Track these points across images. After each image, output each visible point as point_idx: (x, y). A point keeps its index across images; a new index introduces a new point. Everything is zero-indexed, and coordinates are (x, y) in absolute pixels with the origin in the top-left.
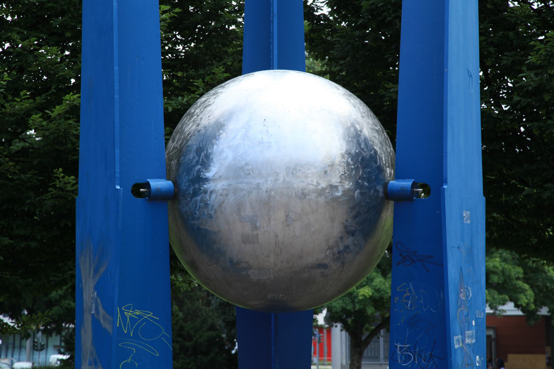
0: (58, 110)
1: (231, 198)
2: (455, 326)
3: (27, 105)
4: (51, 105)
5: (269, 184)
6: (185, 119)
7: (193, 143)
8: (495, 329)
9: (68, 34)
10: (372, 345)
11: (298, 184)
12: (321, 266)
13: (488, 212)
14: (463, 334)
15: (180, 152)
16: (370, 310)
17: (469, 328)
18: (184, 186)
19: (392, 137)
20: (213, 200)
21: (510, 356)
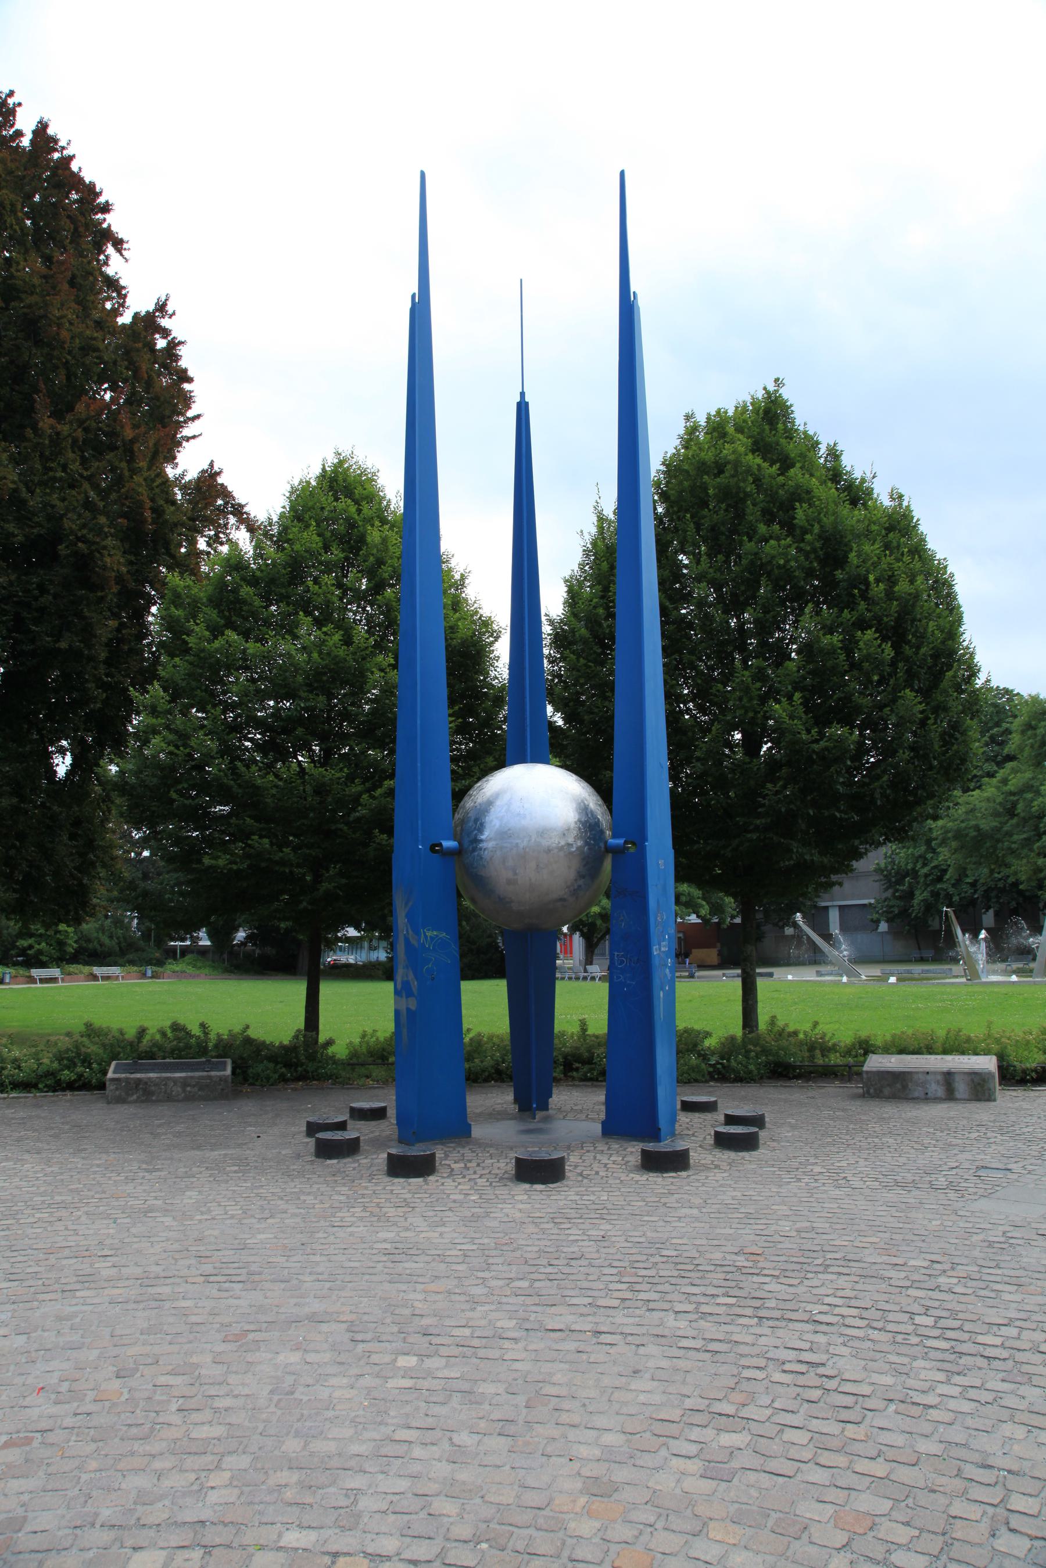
0: (379, 791)
1: (498, 853)
2: (654, 937)
3: (359, 788)
4: (375, 788)
5: (525, 843)
6: (466, 798)
7: (472, 815)
8: (684, 932)
9: (387, 740)
10: (600, 946)
11: (545, 843)
12: (562, 900)
13: (676, 858)
14: (659, 945)
15: (463, 822)
16: (599, 922)
17: (664, 940)
18: (466, 844)
19: (610, 810)
20: (486, 855)
21: (694, 950)
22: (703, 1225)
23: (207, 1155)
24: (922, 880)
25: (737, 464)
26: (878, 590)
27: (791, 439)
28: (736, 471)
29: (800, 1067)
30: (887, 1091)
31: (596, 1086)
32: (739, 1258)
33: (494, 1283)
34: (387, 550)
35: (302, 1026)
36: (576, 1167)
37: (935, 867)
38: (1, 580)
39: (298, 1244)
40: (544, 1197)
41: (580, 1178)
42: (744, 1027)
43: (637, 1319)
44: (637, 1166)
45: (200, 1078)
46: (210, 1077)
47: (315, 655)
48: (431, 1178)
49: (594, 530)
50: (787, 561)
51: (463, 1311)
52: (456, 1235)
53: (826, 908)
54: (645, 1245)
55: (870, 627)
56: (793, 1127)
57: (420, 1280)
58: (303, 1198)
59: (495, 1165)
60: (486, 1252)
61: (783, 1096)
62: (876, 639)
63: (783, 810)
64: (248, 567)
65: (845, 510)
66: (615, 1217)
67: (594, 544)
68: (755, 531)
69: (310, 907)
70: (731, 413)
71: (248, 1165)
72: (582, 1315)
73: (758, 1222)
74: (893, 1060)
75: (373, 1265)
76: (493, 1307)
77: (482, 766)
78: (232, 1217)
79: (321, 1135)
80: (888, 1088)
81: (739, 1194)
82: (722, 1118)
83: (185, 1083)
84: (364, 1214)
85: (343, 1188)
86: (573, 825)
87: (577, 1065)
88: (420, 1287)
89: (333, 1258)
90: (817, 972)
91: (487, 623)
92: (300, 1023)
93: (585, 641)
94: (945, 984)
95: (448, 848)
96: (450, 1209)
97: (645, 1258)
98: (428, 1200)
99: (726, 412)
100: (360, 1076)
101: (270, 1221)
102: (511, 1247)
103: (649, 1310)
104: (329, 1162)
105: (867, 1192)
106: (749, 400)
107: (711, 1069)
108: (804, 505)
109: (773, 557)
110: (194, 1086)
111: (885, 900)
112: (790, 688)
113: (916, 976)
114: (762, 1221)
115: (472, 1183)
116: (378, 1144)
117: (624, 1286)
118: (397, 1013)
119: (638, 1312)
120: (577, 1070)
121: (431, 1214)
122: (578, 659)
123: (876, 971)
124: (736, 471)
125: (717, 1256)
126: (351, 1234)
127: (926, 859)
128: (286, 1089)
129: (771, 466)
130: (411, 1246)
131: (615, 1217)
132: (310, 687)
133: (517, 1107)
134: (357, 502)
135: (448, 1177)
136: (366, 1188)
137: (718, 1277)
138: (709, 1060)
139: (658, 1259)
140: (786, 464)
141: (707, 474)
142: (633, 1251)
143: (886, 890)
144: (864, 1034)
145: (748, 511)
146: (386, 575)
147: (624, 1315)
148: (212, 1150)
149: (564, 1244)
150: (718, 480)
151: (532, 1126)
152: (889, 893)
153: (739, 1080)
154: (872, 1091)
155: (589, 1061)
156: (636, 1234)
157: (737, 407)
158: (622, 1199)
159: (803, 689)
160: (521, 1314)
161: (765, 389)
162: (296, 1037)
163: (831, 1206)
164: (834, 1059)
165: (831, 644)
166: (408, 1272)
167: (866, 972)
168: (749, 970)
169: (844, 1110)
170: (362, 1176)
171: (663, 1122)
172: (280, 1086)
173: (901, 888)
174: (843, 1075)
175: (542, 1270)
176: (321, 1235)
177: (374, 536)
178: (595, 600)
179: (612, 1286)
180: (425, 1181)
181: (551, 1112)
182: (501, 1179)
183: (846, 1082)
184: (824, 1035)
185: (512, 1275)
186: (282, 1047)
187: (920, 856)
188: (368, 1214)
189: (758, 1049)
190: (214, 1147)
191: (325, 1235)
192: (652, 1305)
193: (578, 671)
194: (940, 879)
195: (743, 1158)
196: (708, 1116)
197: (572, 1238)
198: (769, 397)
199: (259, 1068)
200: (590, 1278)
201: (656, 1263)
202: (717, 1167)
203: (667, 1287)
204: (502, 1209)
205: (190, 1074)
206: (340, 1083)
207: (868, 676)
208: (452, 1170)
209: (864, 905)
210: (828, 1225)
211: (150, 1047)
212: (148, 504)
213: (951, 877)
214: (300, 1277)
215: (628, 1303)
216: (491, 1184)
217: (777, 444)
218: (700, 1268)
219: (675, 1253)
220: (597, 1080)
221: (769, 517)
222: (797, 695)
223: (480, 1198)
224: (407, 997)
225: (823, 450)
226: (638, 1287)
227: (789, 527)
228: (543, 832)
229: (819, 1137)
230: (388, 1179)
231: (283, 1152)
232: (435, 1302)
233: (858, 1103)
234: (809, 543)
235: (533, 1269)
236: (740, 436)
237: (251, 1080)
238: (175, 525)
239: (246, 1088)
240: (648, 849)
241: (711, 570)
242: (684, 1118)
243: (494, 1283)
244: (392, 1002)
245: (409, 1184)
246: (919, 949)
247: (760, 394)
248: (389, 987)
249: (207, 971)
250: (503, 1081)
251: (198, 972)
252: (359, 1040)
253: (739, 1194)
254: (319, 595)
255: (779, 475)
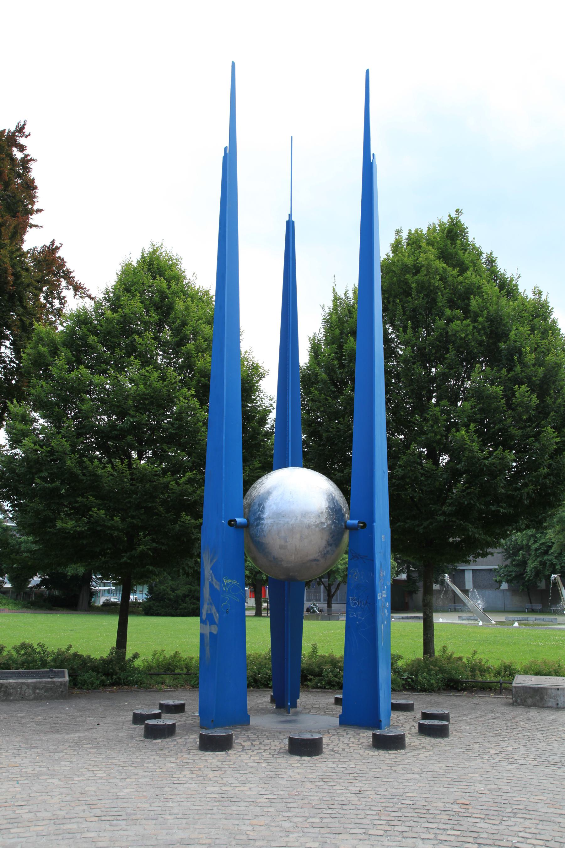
1: (275, 527)
2: (378, 589)
3: (169, 479)
5: (293, 521)
11: (306, 521)
12: (315, 560)
14: (381, 593)
15: (250, 506)
18: (252, 521)
20: (266, 528)
22: (424, 785)
23: (66, 737)
24: (533, 553)
25: (429, 267)
26: (531, 358)
27: (466, 250)
28: (428, 272)
29: (466, 682)
30: (529, 701)
31: (325, 692)
32: (455, 807)
33: (296, 820)
34: (188, 315)
35: (114, 644)
36: (328, 745)
37: (543, 544)
38: (564, 514)
39: (154, 795)
40: (312, 765)
41: (333, 753)
42: (425, 652)
43: (399, 843)
44: (369, 746)
45: (46, 683)
46: (53, 682)
47: (142, 386)
48: (230, 752)
49: (331, 305)
50: (467, 335)
51: (281, 837)
52: (260, 789)
53: (463, 571)
54: (388, 797)
55: (523, 383)
56: (469, 723)
57: (246, 817)
58: (146, 765)
59: (272, 743)
60: (284, 800)
61: (456, 702)
62: (527, 391)
63: (466, 503)
64: (91, 323)
65: (503, 301)
66: (364, 779)
67: (331, 314)
68: (443, 313)
69: (129, 561)
70: (425, 232)
71: (98, 743)
72: (360, 840)
73: (461, 783)
74: (533, 679)
75: (211, 808)
76: (300, 835)
77: (251, 467)
78: (101, 778)
79: (148, 722)
80: (530, 699)
81: (444, 766)
82: (419, 715)
83: (35, 687)
84: (192, 775)
85: (171, 759)
86: (324, 510)
87: (311, 677)
88: (247, 822)
89: (182, 804)
90: (459, 617)
91: (256, 368)
92: (113, 643)
93: (325, 382)
94: (554, 629)
95: (240, 523)
96: (250, 772)
97: (391, 805)
98: (233, 766)
99: (422, 231)
100: (157, 683)
101: (128, 780)
102: (300, 797)
103: (404, 837)
104: (155, 741)
105: (531, 767)
106: (437, 223)
107: (404, 682)
108: (477, 297)
109: (457, 332)
110: (42, 689)
111: (506, 567)
112: (466, 420)
113: (531, 622)
114: (464, 783)
115: (260, 755)
116: (189, 729)
117: (384, 822)
118: (202, 636)
119: (397, 838)
120: (310, 680)
121: (238, 775)
122: (320, 394)
123: (502, 618)
124: (428, 272)
125: (440, 804)
126: (188, 788)
127: (536, 537)
128: (105, 692)
129: (453, 270)
130: (232, 796)
131: (364, 779)
132: (137, 408)
133: (274, 706)
134: (168, 281)
135: (242, 751)
136: (188, 758)
137: (444, 817)
138: (402, 675)
139: (400, 806)
140: (463, 269)
141: (408, 273)
142: (382, 800)
143: (506, 559)
144: (507, 662)
145: (439, 300)
146: (188, 332)
147: (388, 840)
148: (68, 734)
149: (335, 795)
150: (416, 277)
151: (288, 718)
152: (508, 562)
153: (424, 690)
154: (519, 700)
155: (319, 674)
156: (381, 789)
157: (429, 228)
158: (365, 767)
159: (475, 421)
160: (320, 839)
161: (449, 216)
162: (112, 653)
163: (508, 775)
164: (489, 678)
165: (496, 392)
166: (236, 812)
167: (495, 618)
168: (428, 613)
169: (501, 713)
170: (181, 750)
171: (383, 717)
172: (101, 689)
173: (517, 558)
174: (496, 689)
175: (325, 811)
176: (167, 789)
177: (180, 305)
178: (333, 355)
179: (376, 822)
180: (227, 754)
181: (298, 709)
182: (279, 753)
183: (498, 694)
184: (481, 660)
185: (307, 815)
186: (102, 659)
187: (532, 535)
188: (195, 775)
189: (437, 668)
190: (69, 732)
191: (171, 789)
192: (405, 834)
193: (320, 402)
194: (546, 553)
195: (440, 742)
196: (409, 714)
197: (338, 791)
198: (452, 222)
199: (86, 676)
200: (359, 817)
201: (401, 808)
202: (423, 747)
203: (412, 824)
204: (286, 772)
205: (39, 680)
206: (144, 688)
207: (520, 415)
208: (244, 746)
209: (491, 570)
210: (509, 788)
211: (7, 660)
212: (10, 270)
213: (555, 552)
214: (163, 816)
215: (389, 833)
216: (273, 756)
217: (456, 254)
218: (430, 812)
219: (411, 802)
220: (325, 688)
221: (452, 305)
222: (472, 425)
223: (268, 765)
224: (210, 625)
225: (484, 258)
226: (392, 823)
227: (466, 311)
228: (305, 514)
229: (488, 730)
230: (200, 753)
231: (120, 735)
232: (260, 831)
233: (510, 708)
234: (481, 323)
235: (320, 811)
236: (430, 248)
237: (79, 685)
238: (28, 286)
239: (76, 691)
240: (375, 527)
241: (414, 338)
242: (394, 715)
243: (296, 820)
244: (199, 628)
245: (217, 756)
246: (531, 603)
247: (446, 220)
248: (198, 619)
249: (10, 607)
250: (258, 687)
251: (3, 607)
252: (151, 657)
253: (444, 766)
254: (142, 345)
255: (458, 276)
